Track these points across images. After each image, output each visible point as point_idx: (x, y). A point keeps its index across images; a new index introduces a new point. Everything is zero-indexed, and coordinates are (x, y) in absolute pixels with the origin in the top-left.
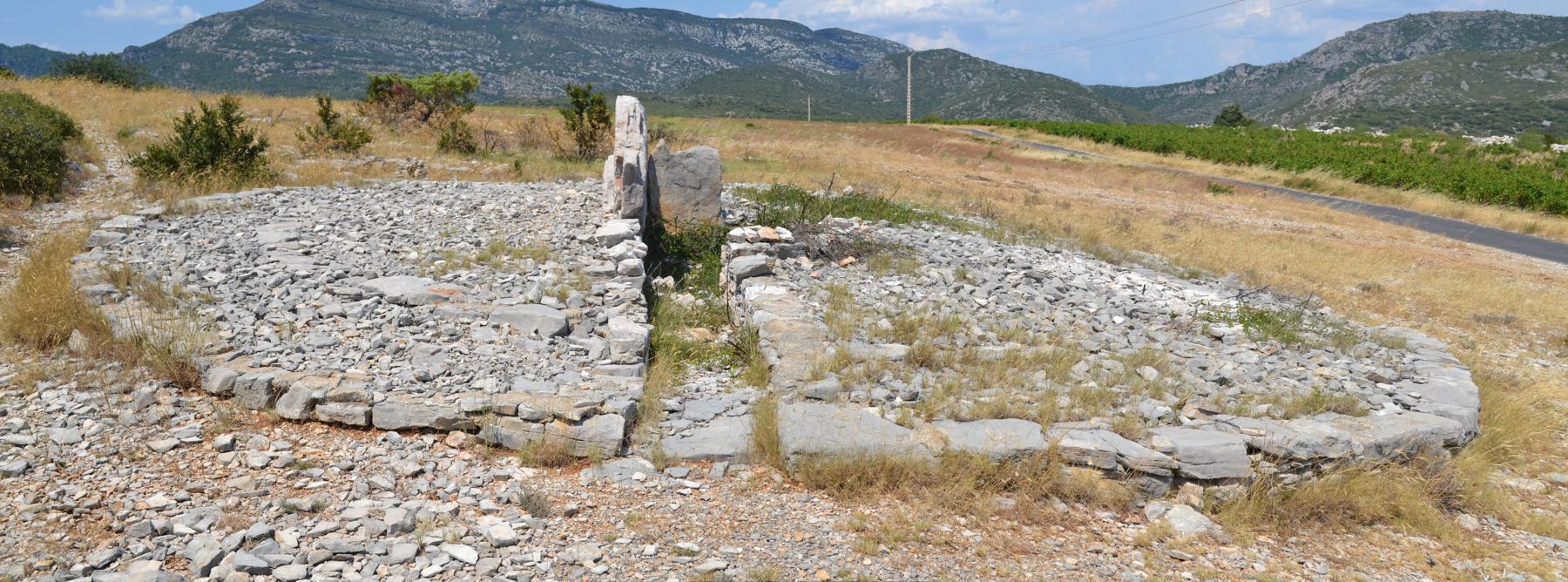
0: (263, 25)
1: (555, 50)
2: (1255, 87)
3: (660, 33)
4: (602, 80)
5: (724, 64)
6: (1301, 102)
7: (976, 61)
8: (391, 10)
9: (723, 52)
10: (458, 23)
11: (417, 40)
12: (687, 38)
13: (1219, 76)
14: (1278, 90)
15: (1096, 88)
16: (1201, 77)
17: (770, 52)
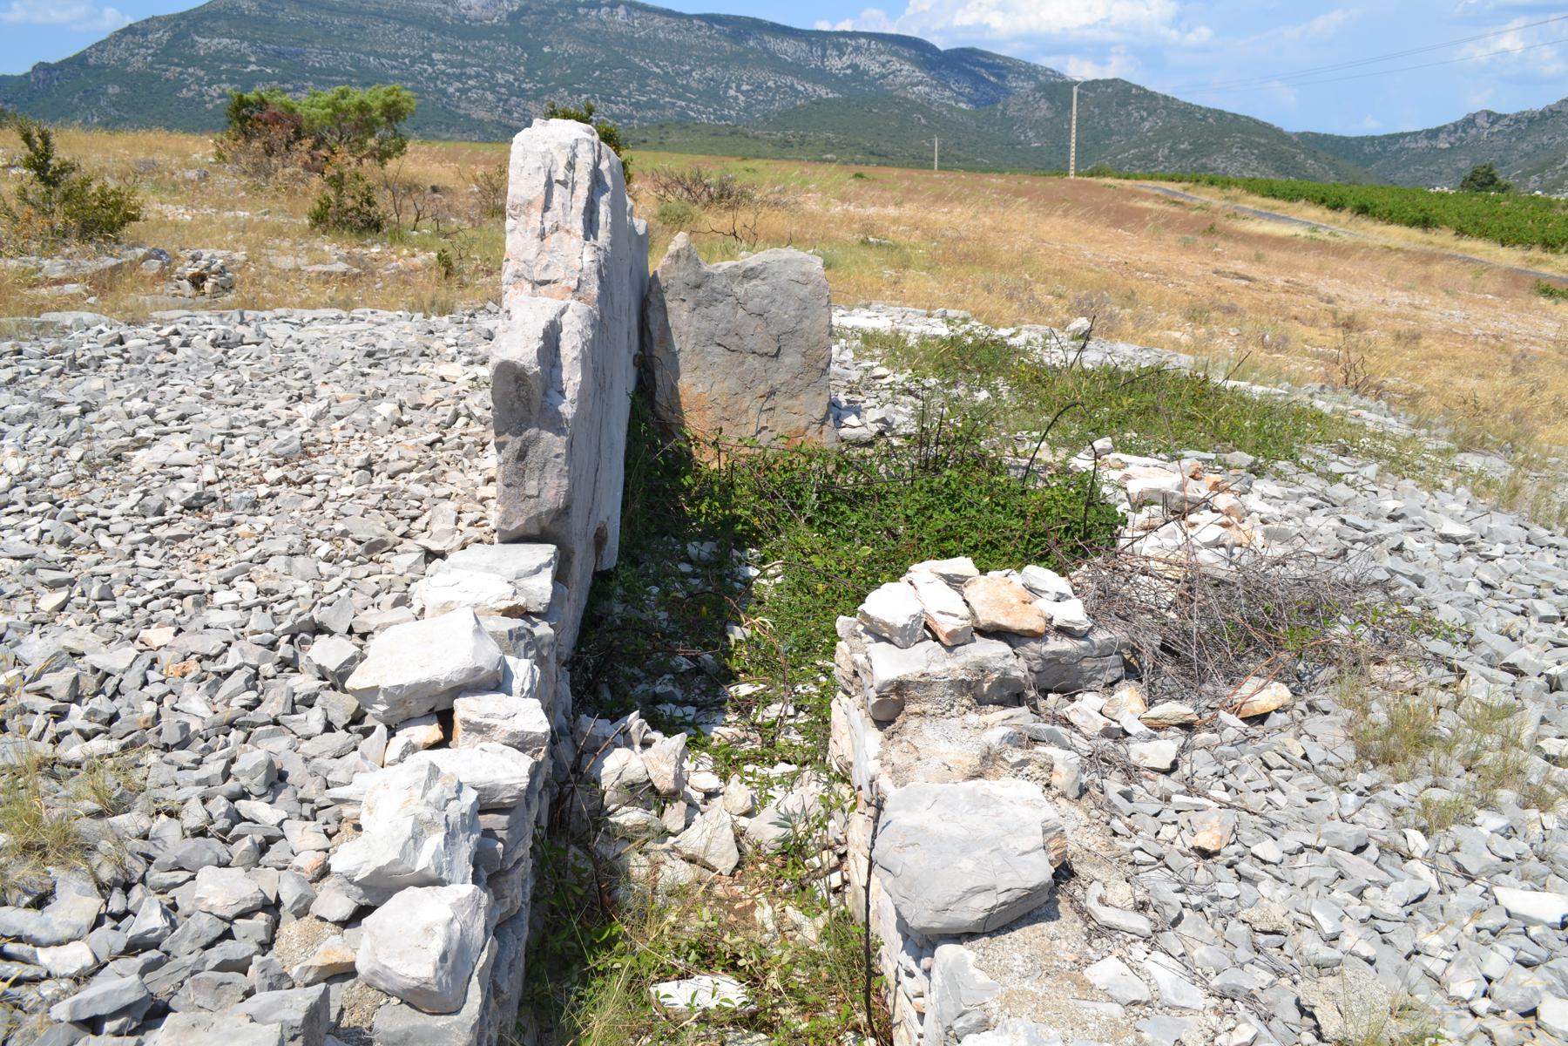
0: (213, 32)
1: (600, 66)
2: (1499, 142)
3: (736, 48)
4: (663, 107)
5: (823, 92)
6: (1553, 163)
7: (1152, 96)
8: (379, 14)
9: (821, 76)
10: (466, 29)
11: (417, 52)
12: (773, 56)
13: (1455, 125)
14: (1526, 146)
15: (1304, 136)
16: (1433, 126)
17: (884, 76)
